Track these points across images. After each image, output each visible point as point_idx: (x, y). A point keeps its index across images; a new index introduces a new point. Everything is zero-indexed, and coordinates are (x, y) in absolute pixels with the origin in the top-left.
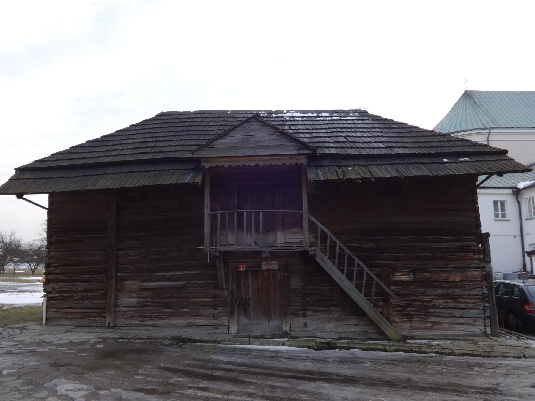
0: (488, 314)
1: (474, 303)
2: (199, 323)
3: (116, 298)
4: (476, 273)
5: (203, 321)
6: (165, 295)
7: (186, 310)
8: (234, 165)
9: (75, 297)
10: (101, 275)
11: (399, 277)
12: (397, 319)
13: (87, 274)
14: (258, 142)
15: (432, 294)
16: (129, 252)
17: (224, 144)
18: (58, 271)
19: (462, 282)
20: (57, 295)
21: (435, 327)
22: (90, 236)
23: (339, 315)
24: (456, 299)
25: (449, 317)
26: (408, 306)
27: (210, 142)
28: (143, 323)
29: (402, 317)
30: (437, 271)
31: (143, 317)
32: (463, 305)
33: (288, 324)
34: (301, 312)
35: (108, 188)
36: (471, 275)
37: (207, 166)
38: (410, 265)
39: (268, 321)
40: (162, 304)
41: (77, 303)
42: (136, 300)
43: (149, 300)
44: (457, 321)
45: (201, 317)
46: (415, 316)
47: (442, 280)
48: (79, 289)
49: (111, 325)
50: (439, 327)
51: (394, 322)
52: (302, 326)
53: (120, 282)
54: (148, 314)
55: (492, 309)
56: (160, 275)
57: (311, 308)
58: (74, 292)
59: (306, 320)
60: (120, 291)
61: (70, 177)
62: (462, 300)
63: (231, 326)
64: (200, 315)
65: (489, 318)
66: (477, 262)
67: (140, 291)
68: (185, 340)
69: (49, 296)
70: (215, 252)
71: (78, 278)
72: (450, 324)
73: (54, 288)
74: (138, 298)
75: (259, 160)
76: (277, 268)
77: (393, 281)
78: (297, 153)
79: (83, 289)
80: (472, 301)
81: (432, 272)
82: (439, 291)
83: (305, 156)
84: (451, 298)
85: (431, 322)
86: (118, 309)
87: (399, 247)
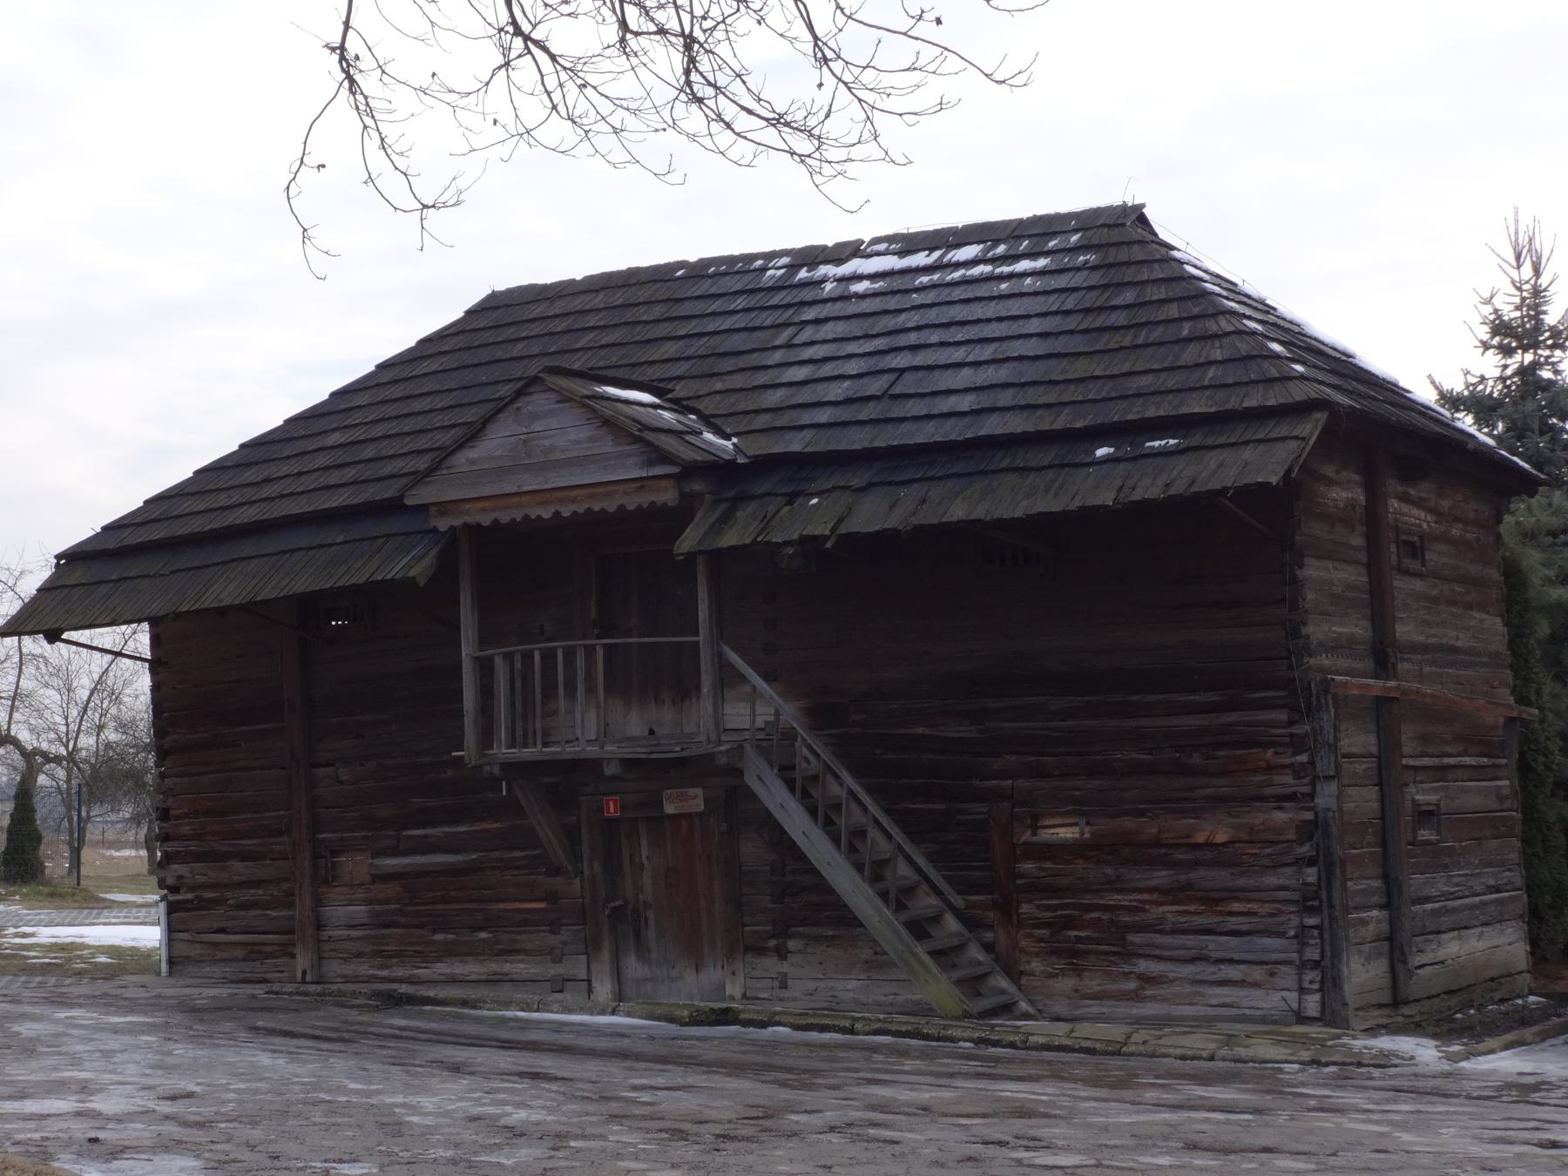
0: (1313, 954)
1: (1272, 915)
2: (517, 973)
3: (318, 902)
4: (1280, 816)
5: (526, 969)
6: (431, 895)
7: (483, 935)
8: (505, 518)
9: (228, 900)
10: (281, 839)
11: (1052, 831)
12: (1036, 965)
13: (250, 838)
14: (552, 449)
15: (1141, 885)
16: (340, 770)
17: (472, 462)
18: (185, 829)
19: (1237, 845)
20: (190, 896)
21: (1148, 993)
22: (250, 728)
23: (876, 953)
24: (1218, 901)
25: (1193, 960)
26: (1069, 923)
27: (443, 456)
28: (384, 973)
29: (1054, 959)
30: (1156, 809)
31: (382, 957)
32: (1234, 922)
33: (740, 978)
34: (773, 943)
35: (223, 604)
36: (1263, 823)
37: (443, 524)
38: (1077, 793)
39: (697, 971)
40: (426, 919)
41: (233, 918)
42: (363, 907)
43: (393, 906)
44: (1213, 973)
45: (521, 957)
46: (1092, 957)
47: (1173, 838)
48: (236, 878)
49: (308, 978)
50: (1160, 992)
51: (1027, 975)
52: (776, 983)
53: (325, 857)
54: (394, 948)
55: (1327, 936)
56: (418, 836)
57: (801, 929)
58: (226, 886)
59: (785, 967)
60: (326, 882)
61: (161, 575)
62: (1236, 906)
63: (594, 984)
64: (518, 952)
65: (1316, 965)
66: (1288, 779)
67: (373, 882)
68: (401, 998)
69: (172, 898)
70: (490, 764)
71: (231, 849)
72: (1194, 982)
73: (180, 877)
74: (369, 902)
75: (561, 500)
76: (703, 807)
77: (1024, 843)
78: (645, 475)
79: (244, 879)
80: (1267, 908)
81: (1142, 813)
82: (1161, 877)
83: (672, 481)
84: (1202, 900)
85: (1403, 1015)
86: (326, 933)
87: (1047, 732)
